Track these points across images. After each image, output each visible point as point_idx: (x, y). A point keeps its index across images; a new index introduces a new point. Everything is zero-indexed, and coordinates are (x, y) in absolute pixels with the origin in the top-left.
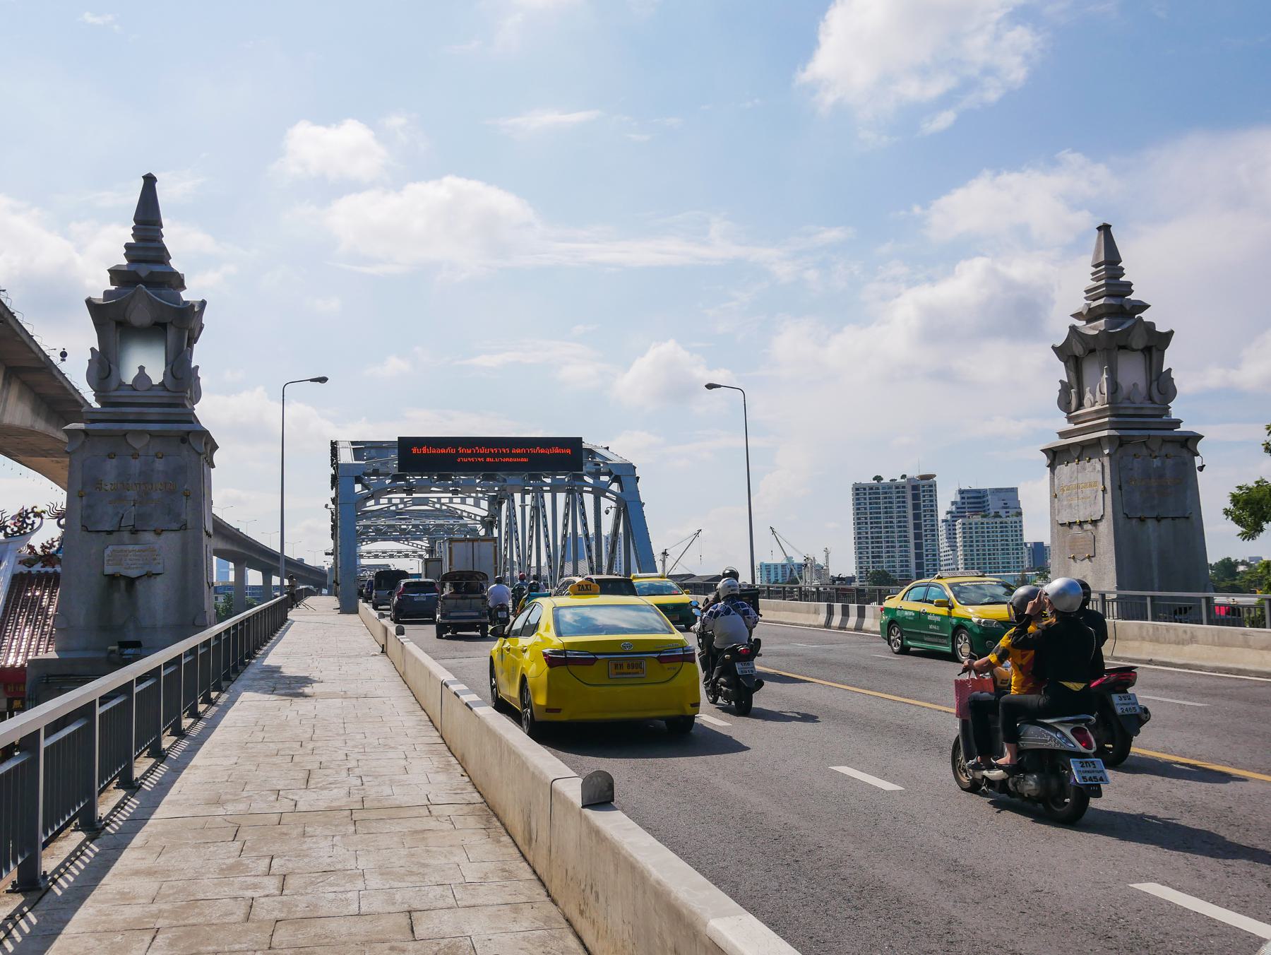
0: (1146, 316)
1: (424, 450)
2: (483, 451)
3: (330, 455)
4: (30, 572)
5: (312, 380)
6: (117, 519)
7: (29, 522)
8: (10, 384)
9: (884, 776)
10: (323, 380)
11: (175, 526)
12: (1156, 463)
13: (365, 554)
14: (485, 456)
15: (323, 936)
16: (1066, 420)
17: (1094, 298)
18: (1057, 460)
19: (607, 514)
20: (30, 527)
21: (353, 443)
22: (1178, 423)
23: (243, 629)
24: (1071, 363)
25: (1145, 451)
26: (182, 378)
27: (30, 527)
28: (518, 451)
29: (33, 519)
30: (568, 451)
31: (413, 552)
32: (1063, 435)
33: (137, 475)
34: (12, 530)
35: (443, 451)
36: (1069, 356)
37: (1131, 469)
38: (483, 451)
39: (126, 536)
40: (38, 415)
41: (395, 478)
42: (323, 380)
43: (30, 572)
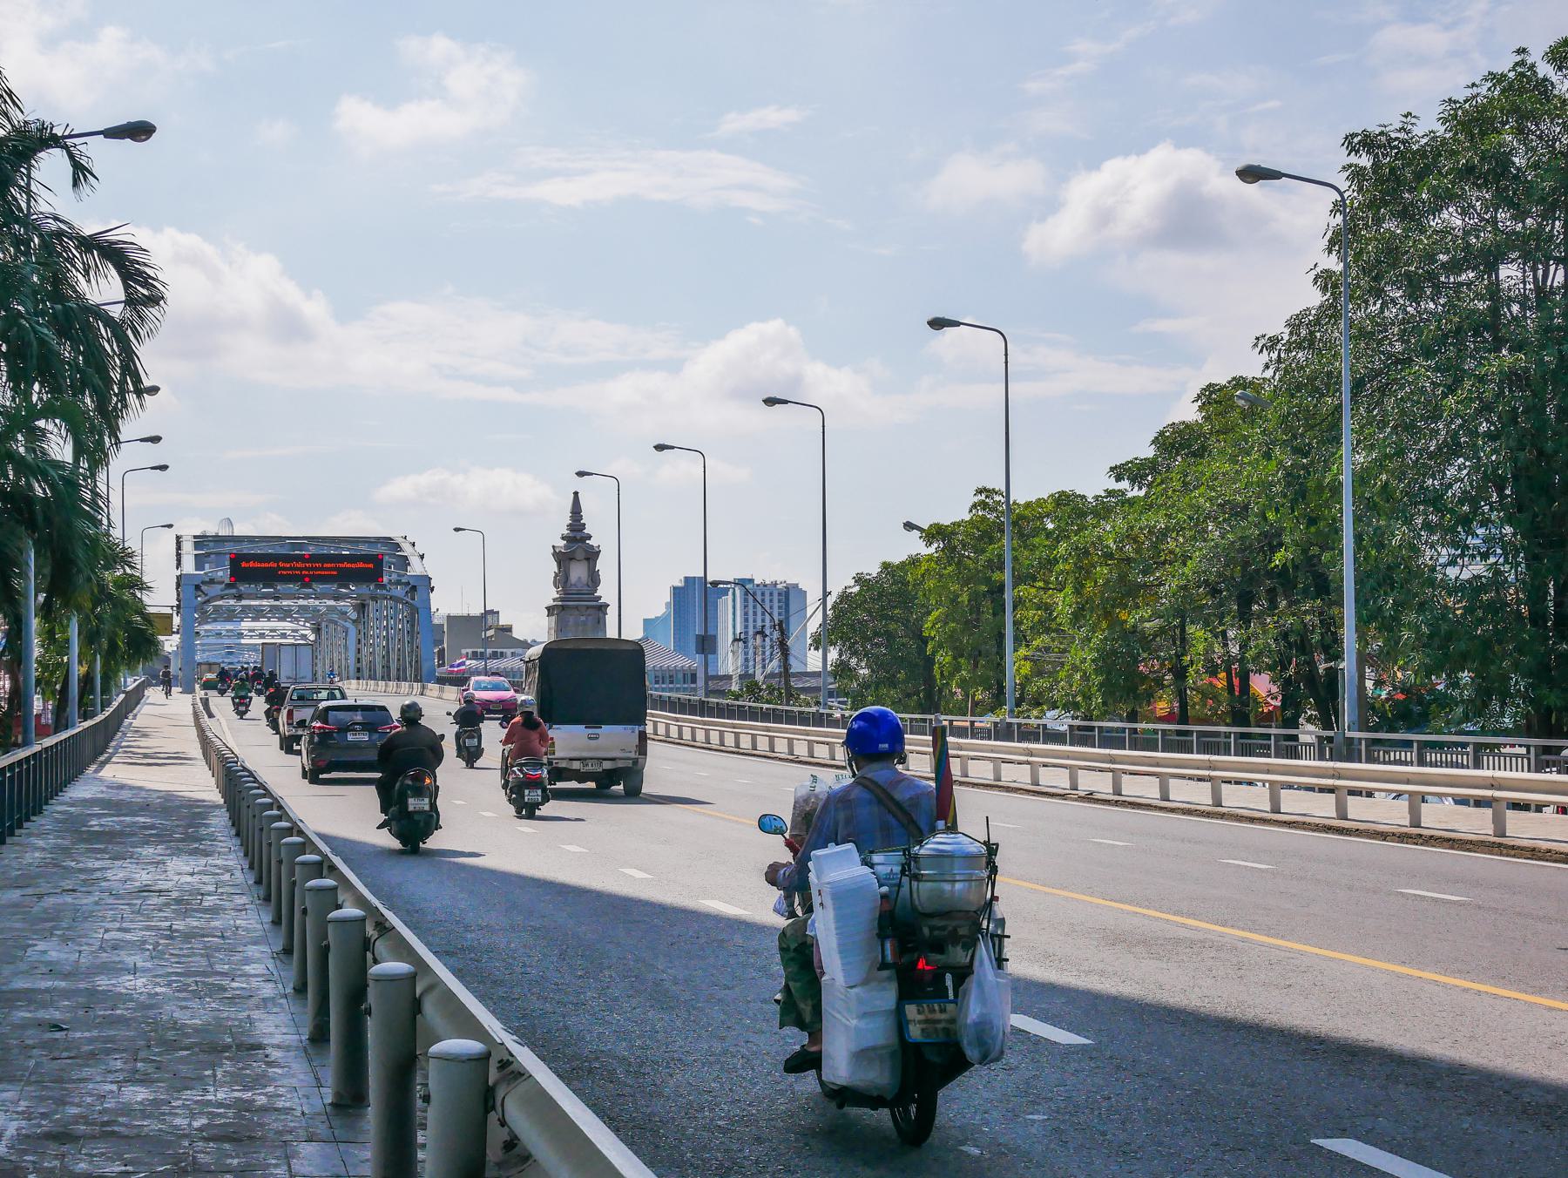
0: (1333, 263)
1: (251, 564)
2: (300, 565)
5: (152, 468)
10: (164, 468)
12: (583, 618)
13: (245, 633)
14: (301, 569)
21: (195, 537)
22: (600, 598)
23: (20, 773)
25: (577, 612)
28: (329, 565)
30: (371, 566)
31: (293, 631)
35: (267, 565)
38: (300, 565)
41: (229, 586)
42: (164, 468)
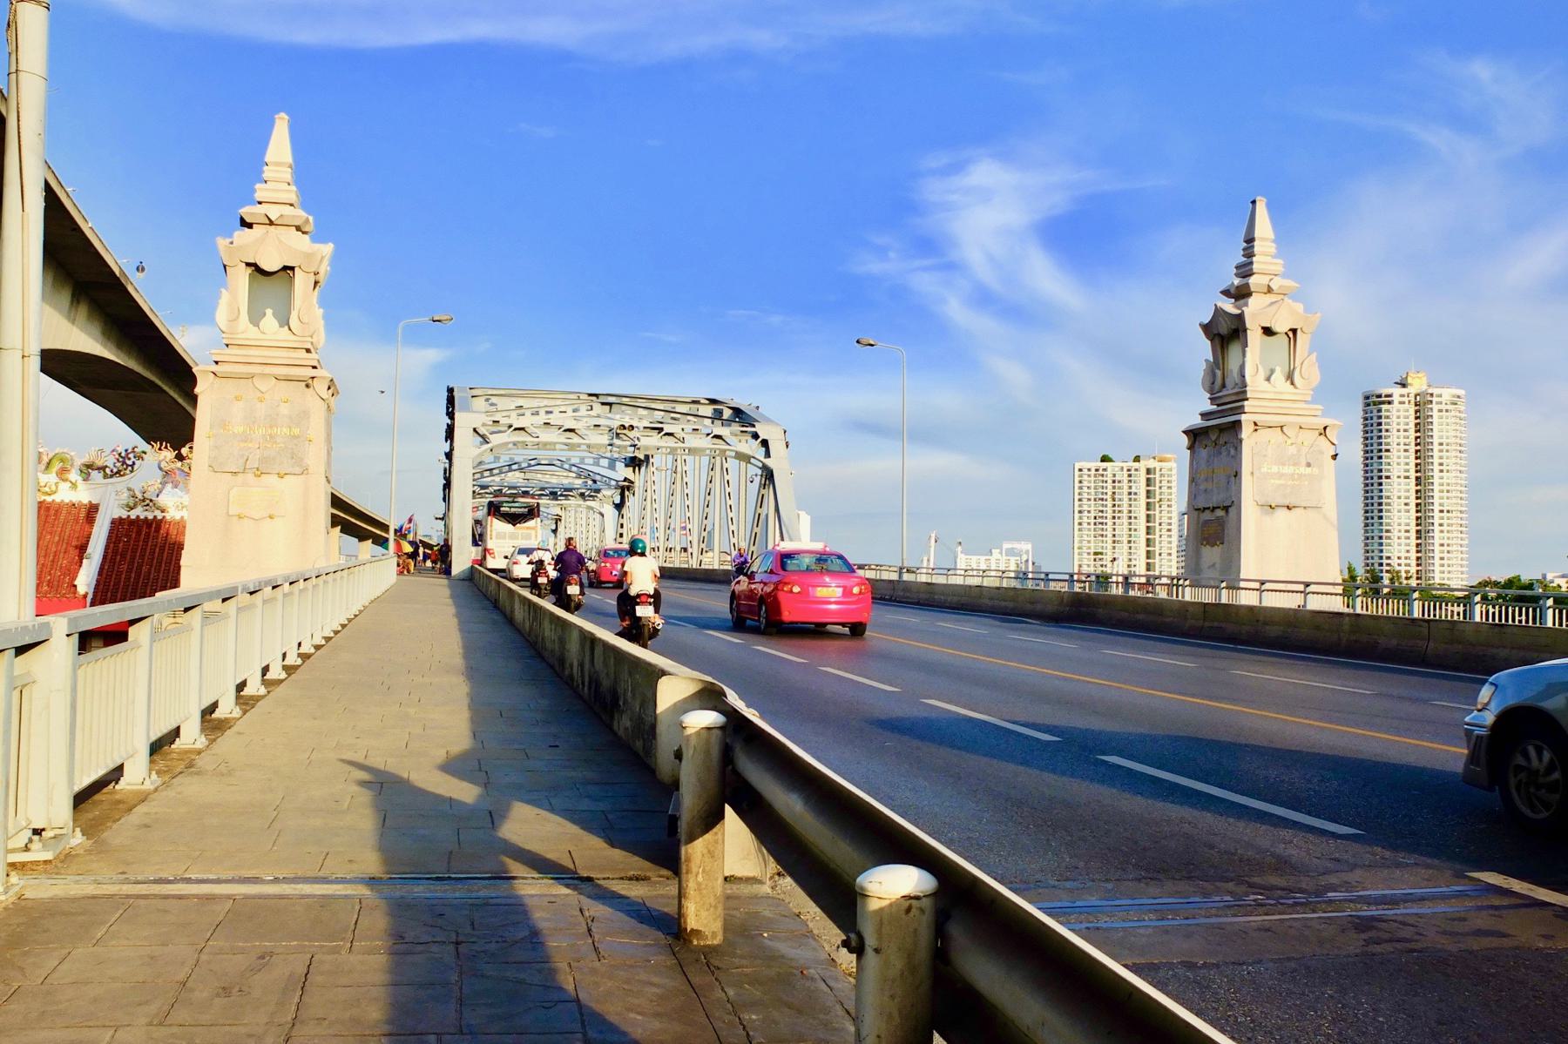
3: (446, 402)
4: (129, 516)
6: (242, 461)
7: (130, 462)
8: (78, 302)
9: (891, 685)
11: (297, 470)
15: (495, 472)
16: (1209, 401)
17: (1243, 275)
18: (1197, 443)
19: (752, 482)
20: (130, 468)
24: (1217, 341)
26: (308, 324)
27: (130, 468)
29: (133, 459)
32: (1205, 415)
33: (262, 418)
34: (112, 471)
36: (1215, 335)
37: (1265, 456)
39: (250, 476)
40: (109, 339)
43: (129, 516)
